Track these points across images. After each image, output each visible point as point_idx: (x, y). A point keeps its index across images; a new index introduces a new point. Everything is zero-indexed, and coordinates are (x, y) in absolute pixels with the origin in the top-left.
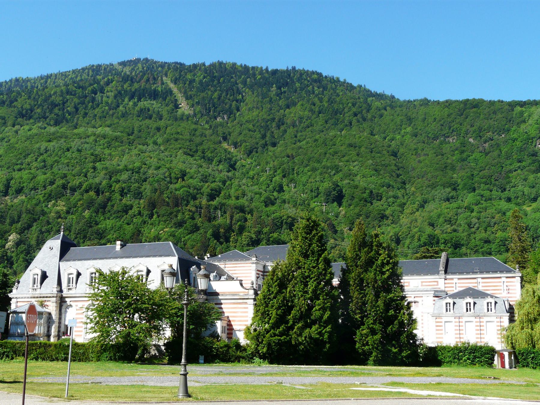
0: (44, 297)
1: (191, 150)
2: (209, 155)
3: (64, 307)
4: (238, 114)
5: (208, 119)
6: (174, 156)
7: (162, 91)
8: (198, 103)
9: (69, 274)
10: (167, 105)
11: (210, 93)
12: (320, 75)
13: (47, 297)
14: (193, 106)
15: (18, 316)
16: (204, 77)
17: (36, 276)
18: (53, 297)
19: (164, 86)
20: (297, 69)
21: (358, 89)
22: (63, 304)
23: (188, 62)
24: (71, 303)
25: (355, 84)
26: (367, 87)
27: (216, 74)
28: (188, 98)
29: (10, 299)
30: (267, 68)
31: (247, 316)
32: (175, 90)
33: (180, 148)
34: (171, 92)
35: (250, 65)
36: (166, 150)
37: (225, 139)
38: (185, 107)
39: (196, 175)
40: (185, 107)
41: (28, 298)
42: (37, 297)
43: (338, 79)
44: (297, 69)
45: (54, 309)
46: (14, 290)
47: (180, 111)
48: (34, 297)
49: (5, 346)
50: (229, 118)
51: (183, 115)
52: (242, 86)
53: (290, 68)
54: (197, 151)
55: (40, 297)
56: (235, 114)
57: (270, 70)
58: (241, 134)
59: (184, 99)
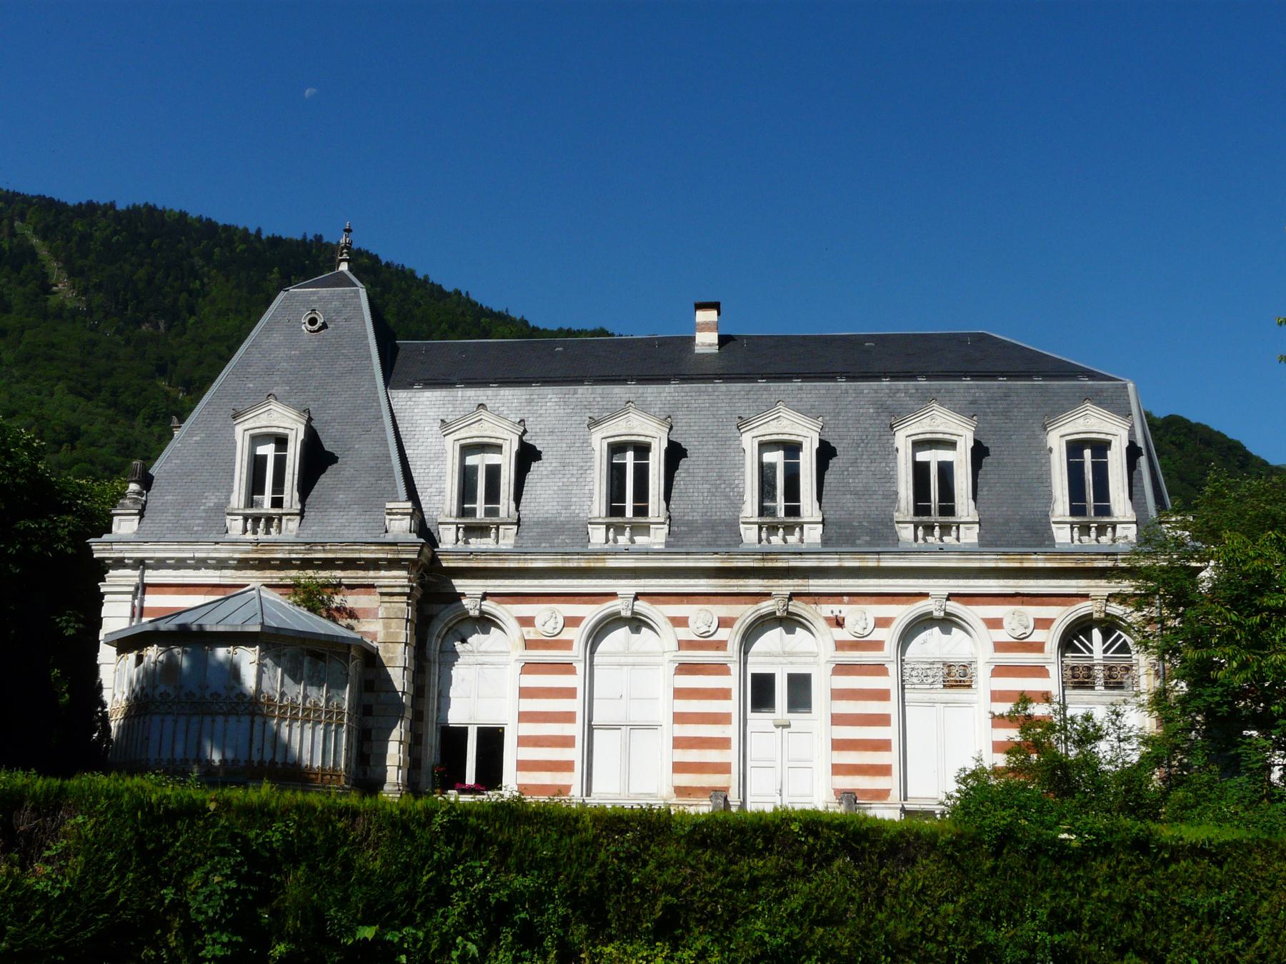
0: (328, 564)
1: (84, 385)
2: (129, 401)
3: (438, 628)
4: (191, 321)
5: (121, 324)
6: (45, 392)
7: (11, 249)
8: (99, 287)
9: (467, 449)
10: (22, 283)
11: (127, 267)
12: (375, 259)
13: (349, 564)
14: (85, 292)
15: (201, 662)
16: (115, 233)
17: (268, 450)
18: (393, 564)
19: (15, 241)
20: (325, 240)
21: (456, 297)
22: (434, 608)
23: (72, 196)
24: (489, 606)
25: (449, 288)
26: (473, 297)
27: (143, 230)
28: (74, 272)
29: (100, 569)
30: (259, 231)
31: (837, 720)
32: (43, 253)
33: (59, 379)
34: (32, 254)
35: (221, 220)
36: (25, 377)
37: (162, 370)
38: (64, 290)
39: (103, 441)
40: (64, 290)
41: (221, 564)
42: (285, 564)
43: (412, 272)
44: (325, 240)
45: (402, 632)
46: (125, 526)
47: (53, 301)
48: (263, 564)
49: (505, 849)
50: (168, 329)
51: (62, 307)
52: (201, 262)
53: (310, 237)
54: (98, 389)
55: (306, 564)
56: (184, 321)
57: (264, 237)
58: (201, 363)
59: (65, 275)
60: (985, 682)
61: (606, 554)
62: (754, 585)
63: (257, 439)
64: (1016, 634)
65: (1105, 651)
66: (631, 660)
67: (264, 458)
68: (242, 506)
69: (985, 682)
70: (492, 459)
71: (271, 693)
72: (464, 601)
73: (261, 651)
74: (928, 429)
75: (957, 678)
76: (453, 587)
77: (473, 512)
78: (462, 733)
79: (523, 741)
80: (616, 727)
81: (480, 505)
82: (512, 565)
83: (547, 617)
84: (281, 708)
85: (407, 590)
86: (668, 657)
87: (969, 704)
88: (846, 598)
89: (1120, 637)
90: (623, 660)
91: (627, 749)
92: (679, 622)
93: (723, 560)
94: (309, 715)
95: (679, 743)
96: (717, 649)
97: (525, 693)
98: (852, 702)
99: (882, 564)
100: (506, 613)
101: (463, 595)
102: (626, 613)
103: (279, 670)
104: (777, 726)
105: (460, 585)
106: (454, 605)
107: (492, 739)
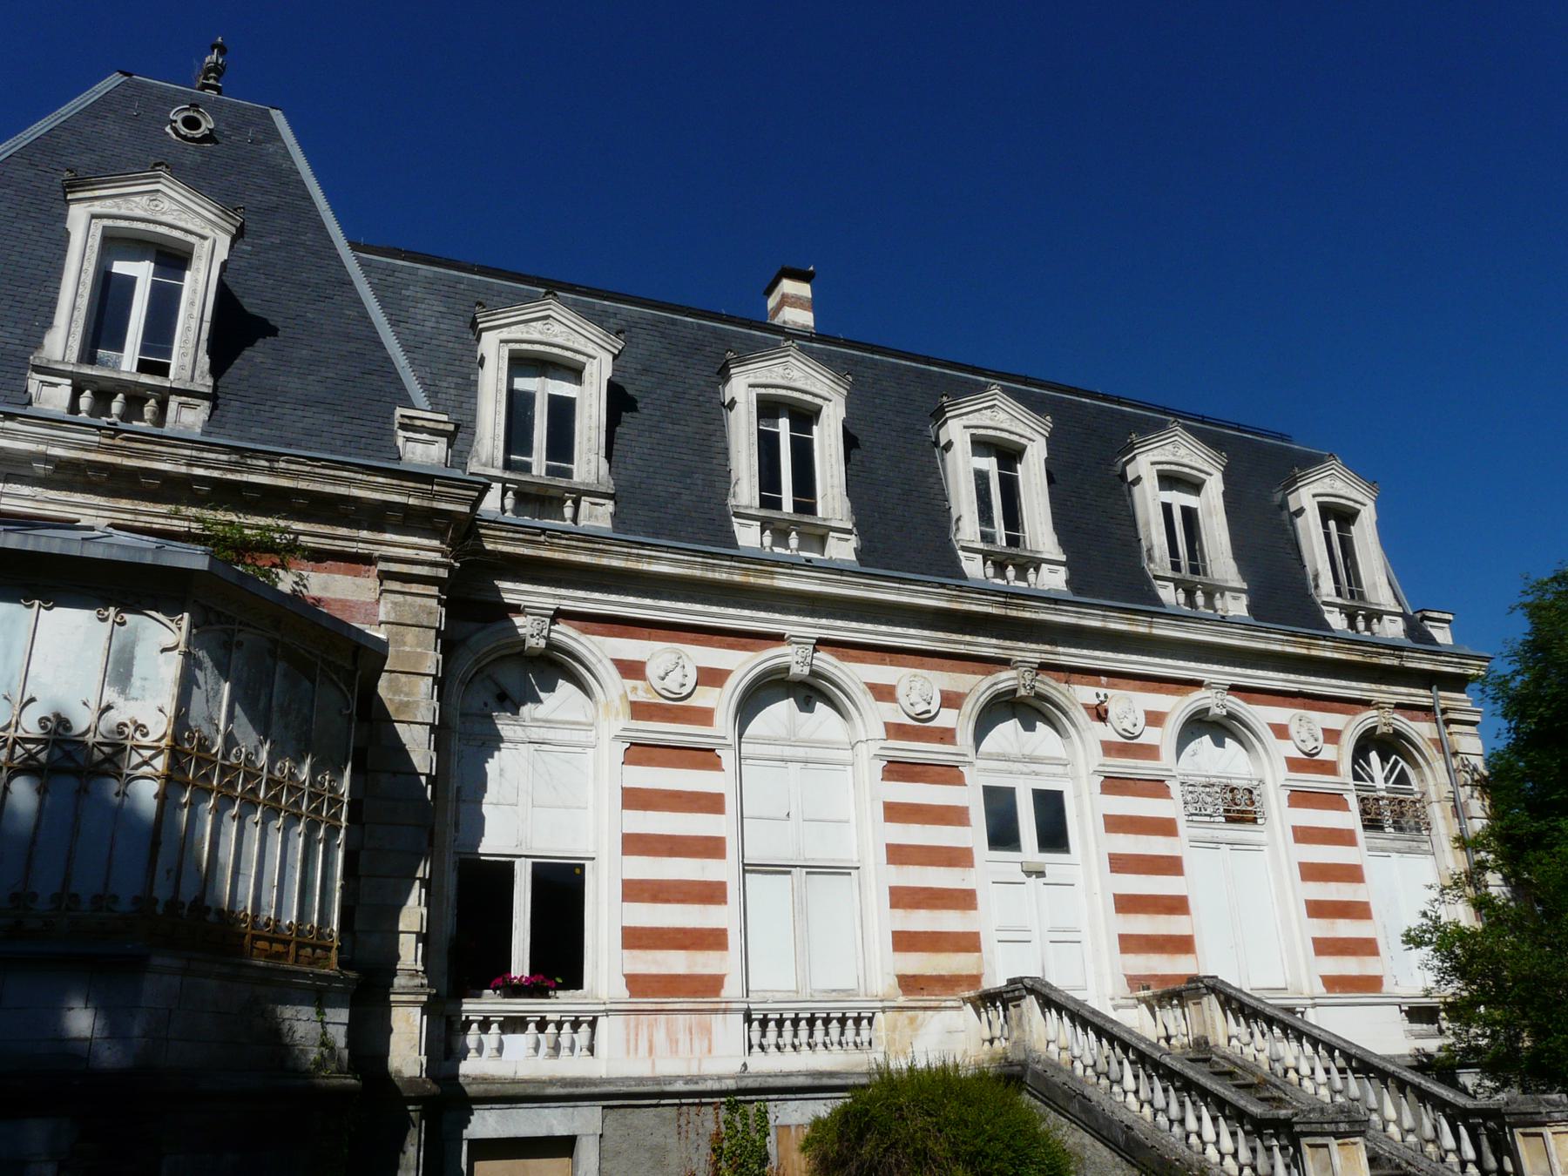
24: (565, 634)
60: (1280, 816)
61: (777, 564)
62: (986, 646)
63: (117, 243)
64: (1308, 747)
65: (1386, 779)
66: (800, 752)
67: (130, 282)
68: (73, 355)
69: (1280, 816)
70: (564, 389)
71: (206, 730)
72: (518, 621)
73: (192, 625)
74: (1171, 458)
75: (1240, 809)
76: (498, 590)
77: (526, 468)
78: (502, 872)
79: (635, 891)
80: (782, 870)
81: (539, 461)
82: (615, 563)
83: (670, 664)
84: (224, 771)
85: (443, 573)
86: (875, 748)
87: (1256, 846)
88: (1104, 679)
89: (1396, 763)
90: (788, 752)
91: (800, 910)
92: (884, 693)
93: (951, 598)
94: (278, 804)
95: (903, 898)
96: (942, 740)
97: (635, 799)
98: (1132, 837)
99: (1155, 631)
100: (600, 650)
101: (517, 609)
102: (799, 671)
103: (227, 687)
104: (1029, 874)
105: (512, 591)
106: (498, 626)
107: (561, 888)
